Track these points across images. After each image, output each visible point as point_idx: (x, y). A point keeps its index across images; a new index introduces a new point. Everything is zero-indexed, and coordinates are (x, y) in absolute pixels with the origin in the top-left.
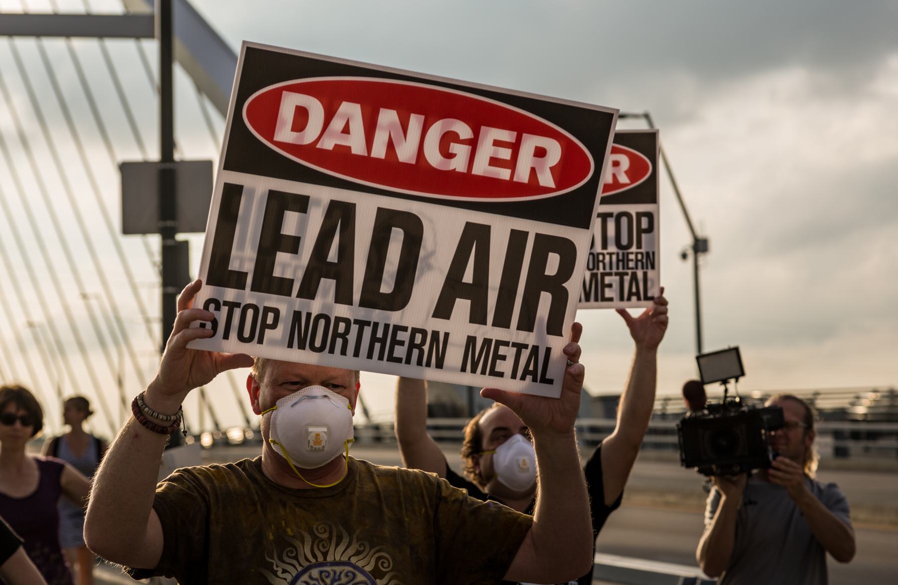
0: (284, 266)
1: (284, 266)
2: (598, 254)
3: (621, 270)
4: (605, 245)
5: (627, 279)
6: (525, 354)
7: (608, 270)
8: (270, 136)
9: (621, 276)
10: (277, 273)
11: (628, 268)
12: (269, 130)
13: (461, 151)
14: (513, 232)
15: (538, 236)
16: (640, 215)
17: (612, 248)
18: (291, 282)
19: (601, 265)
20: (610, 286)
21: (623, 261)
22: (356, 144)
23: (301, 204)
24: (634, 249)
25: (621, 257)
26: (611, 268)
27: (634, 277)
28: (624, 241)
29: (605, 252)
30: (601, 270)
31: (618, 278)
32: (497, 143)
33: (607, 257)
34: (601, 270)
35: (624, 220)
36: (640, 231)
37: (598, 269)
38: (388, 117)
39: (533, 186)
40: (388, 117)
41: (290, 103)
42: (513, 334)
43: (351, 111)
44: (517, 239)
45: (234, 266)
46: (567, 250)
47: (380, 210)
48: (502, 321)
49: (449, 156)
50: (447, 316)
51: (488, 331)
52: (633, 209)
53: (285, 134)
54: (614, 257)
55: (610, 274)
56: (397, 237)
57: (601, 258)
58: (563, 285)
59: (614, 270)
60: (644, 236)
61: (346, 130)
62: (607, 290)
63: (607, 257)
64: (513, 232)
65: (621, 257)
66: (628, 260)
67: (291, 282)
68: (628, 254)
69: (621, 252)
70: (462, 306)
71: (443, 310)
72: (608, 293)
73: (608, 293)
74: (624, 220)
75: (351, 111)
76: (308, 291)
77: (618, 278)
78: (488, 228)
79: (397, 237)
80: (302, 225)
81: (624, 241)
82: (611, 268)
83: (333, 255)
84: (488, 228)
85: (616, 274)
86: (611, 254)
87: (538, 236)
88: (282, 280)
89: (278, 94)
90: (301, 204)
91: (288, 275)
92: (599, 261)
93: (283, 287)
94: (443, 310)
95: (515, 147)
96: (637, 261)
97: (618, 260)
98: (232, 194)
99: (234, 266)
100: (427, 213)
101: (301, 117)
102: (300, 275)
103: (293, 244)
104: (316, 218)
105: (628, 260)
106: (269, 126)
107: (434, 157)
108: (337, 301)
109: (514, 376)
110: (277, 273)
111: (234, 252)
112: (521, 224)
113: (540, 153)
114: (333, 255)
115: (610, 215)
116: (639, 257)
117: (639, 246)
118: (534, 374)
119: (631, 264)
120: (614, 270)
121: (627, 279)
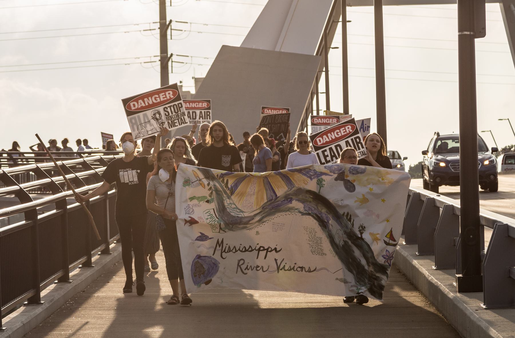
0: (328, 159)
1: (328, 159)
2: (171, 116)
3: (178, 118)
4: (172, 114)
5: (180, 120)
6: (361, 153)
7: (175, 119)
8: (318, 145)
9: (178, 119)
10: (328, 160)
11: (179, 117)
12: (317, 144)
13: (158, 99)
14: (351, 139)
15: (354, 138)
16: (178, 104)
17: (174, 114)
18: (330, 160)
19: (173, 118)
20: (176, 123)
21: (177, 116)
22: (143, 105)
23: (326, 151)
24: (179, 112)
25: (177, 115)
26: (175, 118)
27: (181, 119)
28: (176, 111)
29: (173, 115)
30: (173, 119)
31: (177, 120)
32: (343, 130)
33: (173, 116)
34: (173, 119)
35: (175, 106)
36: (180, 108)
37: (172, 119)
38: (146, 99)
39: (350, 132)
40: (146, 99)
41: (132, 104)
42: (206, 120)
43: (325, 136)
44: (352, 140)
45: (323, 162)
46: (358, 137)
47: (335, 146)
48: (205, 119)
49: (338, 135)
50: (317, 153)
51: (204, 120)
52: (176, 103)
53: (319, 144)
54: (175, 116)
55: (175, 120)
56: (338, 148)
57: (172, 117)
58: (449, 148)
59: (176, 119)
60: (181, 108)
61: (325, 139)
62: (176, 124)
63: (173, 116)
64: (351, 139)
65: (177, 115)
66: (179, 115)
67: (330, 160)
68: (178, 114)
69: (176, 114)
70: (201, 118)
71: (200, 119)
72: (176, 124)
73: (176, 124)
74: (175, 106)
75: (325, 136)
76: (332, 160)
77: (177, 120)
78: (348, 141)
79: (338, 148)
80: (327, 153)
81: (176, 111)
82: (175, 118)
83: (333, 154)
84: (348, 141)
85: (177, 119)
86: (174, 115)
87: (354, 138)
88: (329, 161)
89: (316, 140)
90: (326, 151)
91: (329, 160)
92: (172, 118)
93: (329, 161)
94: (200, 119)
95: (345, 129)
96: (181, 115)
97: (176, 116)
98: (318, 154)
99: (323, 162)
100: (341, 143)
101: (134, 105)
102: (330, 158)
103: (328, 156)
104: (328, 151)
105: (179, 115)
106: (130, 108)
107: (337, 136)
108: (336, 159)
109: (362, 156)
110: (328, 160)
111: (322, 160)
112: (351, 138)
113: (348, 128)
114: (333, 154)
115: (171, 106)
116: (181, 114)
117: (180, 111)
118: (364, 154)
119: (180, 116)
120: (176, 119)
121: (180, 120)
